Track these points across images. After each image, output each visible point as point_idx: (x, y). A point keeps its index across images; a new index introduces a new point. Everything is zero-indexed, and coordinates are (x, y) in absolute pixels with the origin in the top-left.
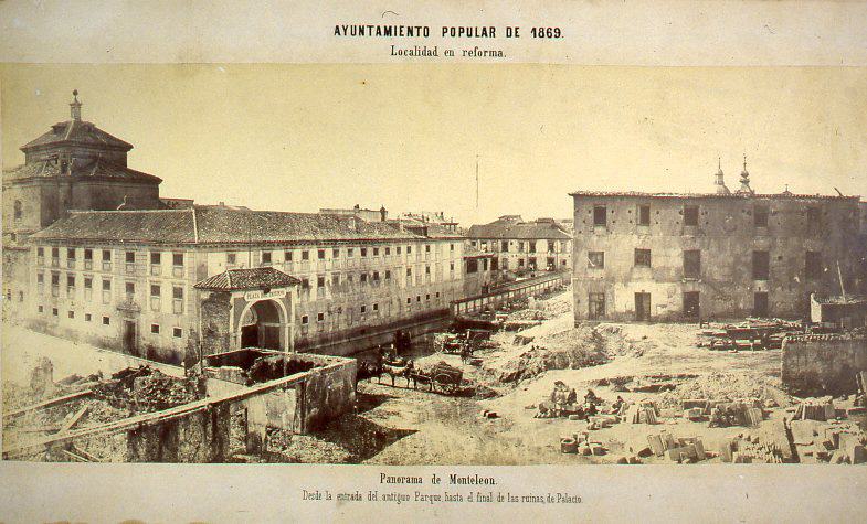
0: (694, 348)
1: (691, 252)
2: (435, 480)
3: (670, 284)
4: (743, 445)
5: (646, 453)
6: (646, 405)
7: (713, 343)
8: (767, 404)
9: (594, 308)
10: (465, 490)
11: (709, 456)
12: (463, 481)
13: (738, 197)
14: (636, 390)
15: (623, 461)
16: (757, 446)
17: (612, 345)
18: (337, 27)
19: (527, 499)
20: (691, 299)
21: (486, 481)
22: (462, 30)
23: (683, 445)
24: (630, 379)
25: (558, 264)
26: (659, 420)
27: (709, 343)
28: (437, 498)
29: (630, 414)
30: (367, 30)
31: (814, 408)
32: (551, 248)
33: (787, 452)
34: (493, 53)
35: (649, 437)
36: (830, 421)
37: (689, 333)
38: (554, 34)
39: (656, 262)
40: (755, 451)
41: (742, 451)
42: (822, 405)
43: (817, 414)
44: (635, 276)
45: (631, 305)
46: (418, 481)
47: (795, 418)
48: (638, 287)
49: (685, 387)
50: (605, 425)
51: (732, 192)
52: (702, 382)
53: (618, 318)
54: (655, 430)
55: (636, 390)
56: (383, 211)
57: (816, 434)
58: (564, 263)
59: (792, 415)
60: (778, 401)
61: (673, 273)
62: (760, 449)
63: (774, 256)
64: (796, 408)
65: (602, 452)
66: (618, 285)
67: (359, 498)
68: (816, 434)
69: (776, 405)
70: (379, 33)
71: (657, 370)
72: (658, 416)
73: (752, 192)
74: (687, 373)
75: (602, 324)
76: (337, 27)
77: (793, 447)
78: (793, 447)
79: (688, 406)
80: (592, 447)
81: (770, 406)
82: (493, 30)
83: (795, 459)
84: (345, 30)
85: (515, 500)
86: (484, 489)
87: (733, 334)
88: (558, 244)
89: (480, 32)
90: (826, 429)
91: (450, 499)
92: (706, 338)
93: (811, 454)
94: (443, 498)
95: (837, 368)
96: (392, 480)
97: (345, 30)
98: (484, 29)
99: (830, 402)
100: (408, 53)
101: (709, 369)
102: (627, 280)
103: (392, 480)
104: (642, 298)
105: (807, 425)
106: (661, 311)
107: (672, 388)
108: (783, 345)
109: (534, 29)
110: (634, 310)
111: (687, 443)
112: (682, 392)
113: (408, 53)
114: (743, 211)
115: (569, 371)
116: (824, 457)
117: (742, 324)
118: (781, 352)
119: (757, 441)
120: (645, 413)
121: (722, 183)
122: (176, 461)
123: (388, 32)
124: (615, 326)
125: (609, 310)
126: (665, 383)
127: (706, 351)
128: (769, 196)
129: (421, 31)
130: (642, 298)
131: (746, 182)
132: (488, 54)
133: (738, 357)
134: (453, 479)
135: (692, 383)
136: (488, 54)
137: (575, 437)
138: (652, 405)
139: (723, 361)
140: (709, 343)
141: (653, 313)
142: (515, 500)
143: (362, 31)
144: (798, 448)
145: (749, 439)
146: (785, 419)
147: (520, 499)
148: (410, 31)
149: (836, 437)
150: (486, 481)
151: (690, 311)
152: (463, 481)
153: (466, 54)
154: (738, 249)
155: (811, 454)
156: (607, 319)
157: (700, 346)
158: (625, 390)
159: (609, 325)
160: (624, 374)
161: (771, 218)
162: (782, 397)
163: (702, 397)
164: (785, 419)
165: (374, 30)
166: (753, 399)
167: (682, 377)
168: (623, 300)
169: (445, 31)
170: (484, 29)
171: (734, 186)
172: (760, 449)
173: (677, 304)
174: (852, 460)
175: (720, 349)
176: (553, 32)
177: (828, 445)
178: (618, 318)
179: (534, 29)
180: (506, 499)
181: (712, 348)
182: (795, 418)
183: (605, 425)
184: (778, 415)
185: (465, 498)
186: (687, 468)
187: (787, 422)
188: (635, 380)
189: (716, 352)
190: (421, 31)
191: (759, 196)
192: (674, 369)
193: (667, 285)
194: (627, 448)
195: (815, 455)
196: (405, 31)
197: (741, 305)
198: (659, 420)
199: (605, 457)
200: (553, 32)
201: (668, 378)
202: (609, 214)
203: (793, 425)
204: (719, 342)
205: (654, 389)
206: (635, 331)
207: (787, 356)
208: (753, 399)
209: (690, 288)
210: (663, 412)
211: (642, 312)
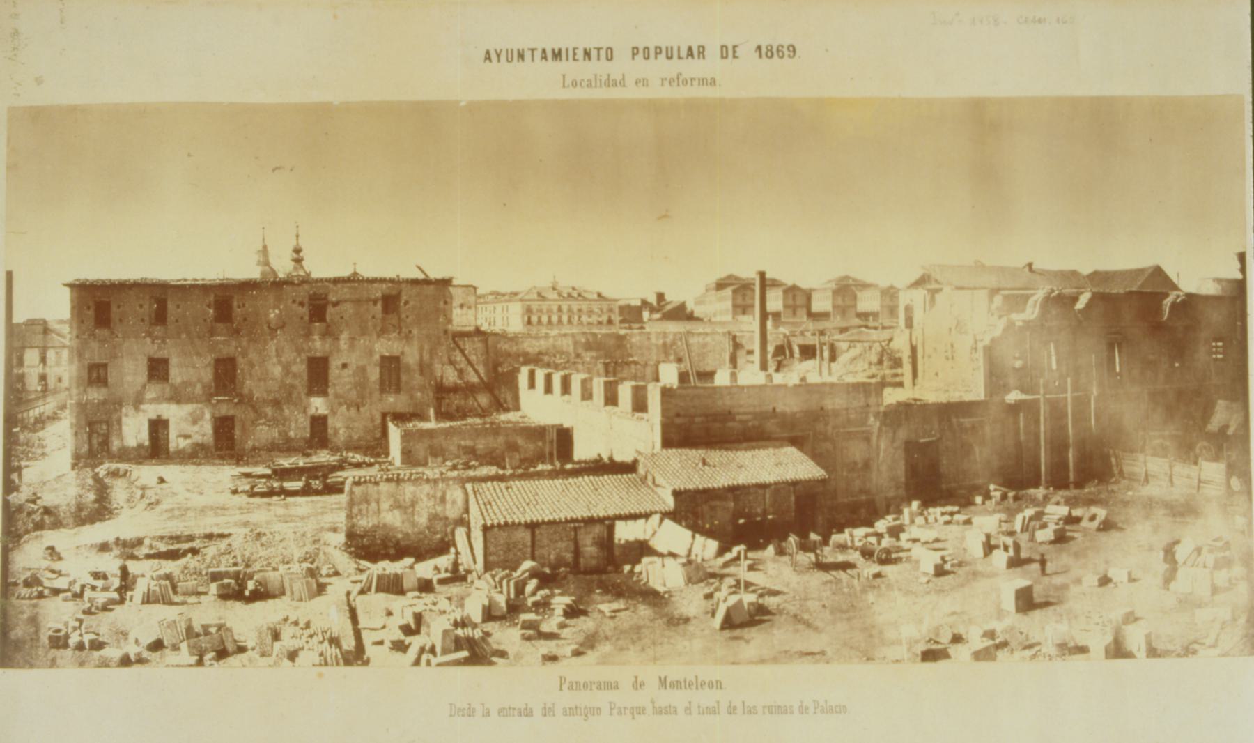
0: (228, 495)
1: (224, 360)
2: (638, 685)
3: (195, 406)
4: (287, 632)
5: (157, 646)
6: (159, 578)
7: (252, 487)
8: (324, 571)
9: (95, 442)
10: (677, 698)
11: (242, 649)
12: (676, 685)
13: (288, 282)
14: (148, 557)
15: (126, 661)
16: (307, 632)
17: (119, 491)
18: (488, 52)
19: (783, 710)
20: (224, 427)
21: (711, 685)
22: (658, 51)
23: (207, 633)
24: (140, 542)
25: (52, 382)
26: (176, 599)
27: (247, 487)
28: (641, 711)
29: (141, 588)
30: (528, 55)
31: (388, 576)
32: (43, 360)
33: (349, 643)
34: (702, 82)
35: (160, 623)
36: (410, 595)
37: (226, 474)
38: (786, 53)
39: (176, 374)
40: (304, 639)
41: (287, 642)
42: (399, 572)
43: (393, 586)
44: (150, 395)
45: (144, 437)
46: (614, 686)
47: (362, 592)
48: (152, 410)
49: (211, 550)
50: (105, 608)
51: (281, 275)
52: (237, 542)
53: (125, 455)
54: (170, 613)
55: (148, 557)
56: (660, 297)
57: (389, 614)
58: (60, 380)
59: (358, 587)
60: (340, 568)
61: (198, 389)
62: (311, 636)
63: (335, 363)
64: (364, 577)
65: (97, 645)
66: (127, 410)
67: (528, 713)
68: (389, 614)
69: (337, 573)
70: (544, 57)
71: (177, 527)
72: (175, 592)
73: (308, 275)
74: (216, 531)
75: (106, 465)
76: (488, 52)
77: (358, 635)
78: (358, 635)
79: (215, 577)
80: (87, 639)
81: (328, 576)
82: (702, 51)
83: (357, 656)
84: (498, 55)
85: (751, 711)
86: (706, 698)
87: (283, 474)
88: (51, 355)
89: (684, 53)
90: (404, 607)
91: (659, 711)
92: (244, 480)
93: (381, 643)
94: (649, 710)
95: (422, 520)
96: (575, 686)
97: (498, 55)
98: (690, 49)
99: (411, 567)
100: (584, 84)
101: (246, 524)
102: (138, 402)
103: (575, 686)
104: (158, 427)
105: (380, 600)
106: (183, 444)
107: (195, 552)
108: (347, 488)
109: (759, 48)
110: (147, 443)
111: (213, 630)
112: (208, 558)
113: (584, 84)
114: (294, 302)
115: (63, 532)
116: (400, 647)
117: (293, 460)
118: (343, 498)
119: (308, 625)
120: (157, 588)
121: (267, 263)
122: (32, 666)
123: (557, 55)
124: (122, 466)
125: (115, 444)
126: (186, 546)
127: (242, 500)
128: (328, 280)
129: (603, 53)
130: (158, 427)
131: (298, 261)
132: (695, 83)
133: (287, 506)
134: (663, 682)
135: (223, 545)
136: (695, 83)
137: (66, 624)
138: (168, 577)
139: (266, 513)
140: (247, 487)
141: (172, 447)
142: (751, 711)
143: (521, 56)
144: (364, 634)
145: (296, 623)
146: (348, 594)
147: (760, 710)
148: (587, 54)
149: (418, 618)
150: (711, 685)
151: (226, 444)
152: (676, 685)
153: (666, 83)
154: (289, 355)
155: (381, 643)
156: (112, 457)
157: (235, 492)
158: (133, 557)
159: (114, 466)
160: (128, 534)
161: (331, 310)
162: (344, 562)
163: (235, 564)
164: (348, 594)
165: (538, 54)
166: (306, 565)
167: (210, 537)
168: (134, 431)
169: (635, 51)
170: (690, 49)
171: (283, 266)
172: (311, 636)
173: (204, 431)
174: (438, 650)
175: (263, 495)
176: (785, 50)
177: (407, 630)
178: (125, 455)
179: (759, 48)
180: (739, 710)
181: (252, 494)
182: (362, 592)
183: (105, 608)
184: (337, 588)
185: (681, 710)
186: (215, 671)
187: (352, 598)
188: (147, 542)
189: (257, 500)
190: (603, 53)
191: (317, 281)
192: (199, 526)
193: (188, 408)
194: (131, 638)
195: (388, 644)
196: (580, 54)
197: (292, 434)
198: (176, 599)
199: (102, 652)
200: (785, 50)
201: (191, 538)
202: (114, 309)
203: (360, 602)
204: (261, 487)
205: (173, 555)
206: (147, 473)
207: (351, 503)
208: (306, 565)
209: (225, 410)
210: (181, 586)
211: (157, 448)
